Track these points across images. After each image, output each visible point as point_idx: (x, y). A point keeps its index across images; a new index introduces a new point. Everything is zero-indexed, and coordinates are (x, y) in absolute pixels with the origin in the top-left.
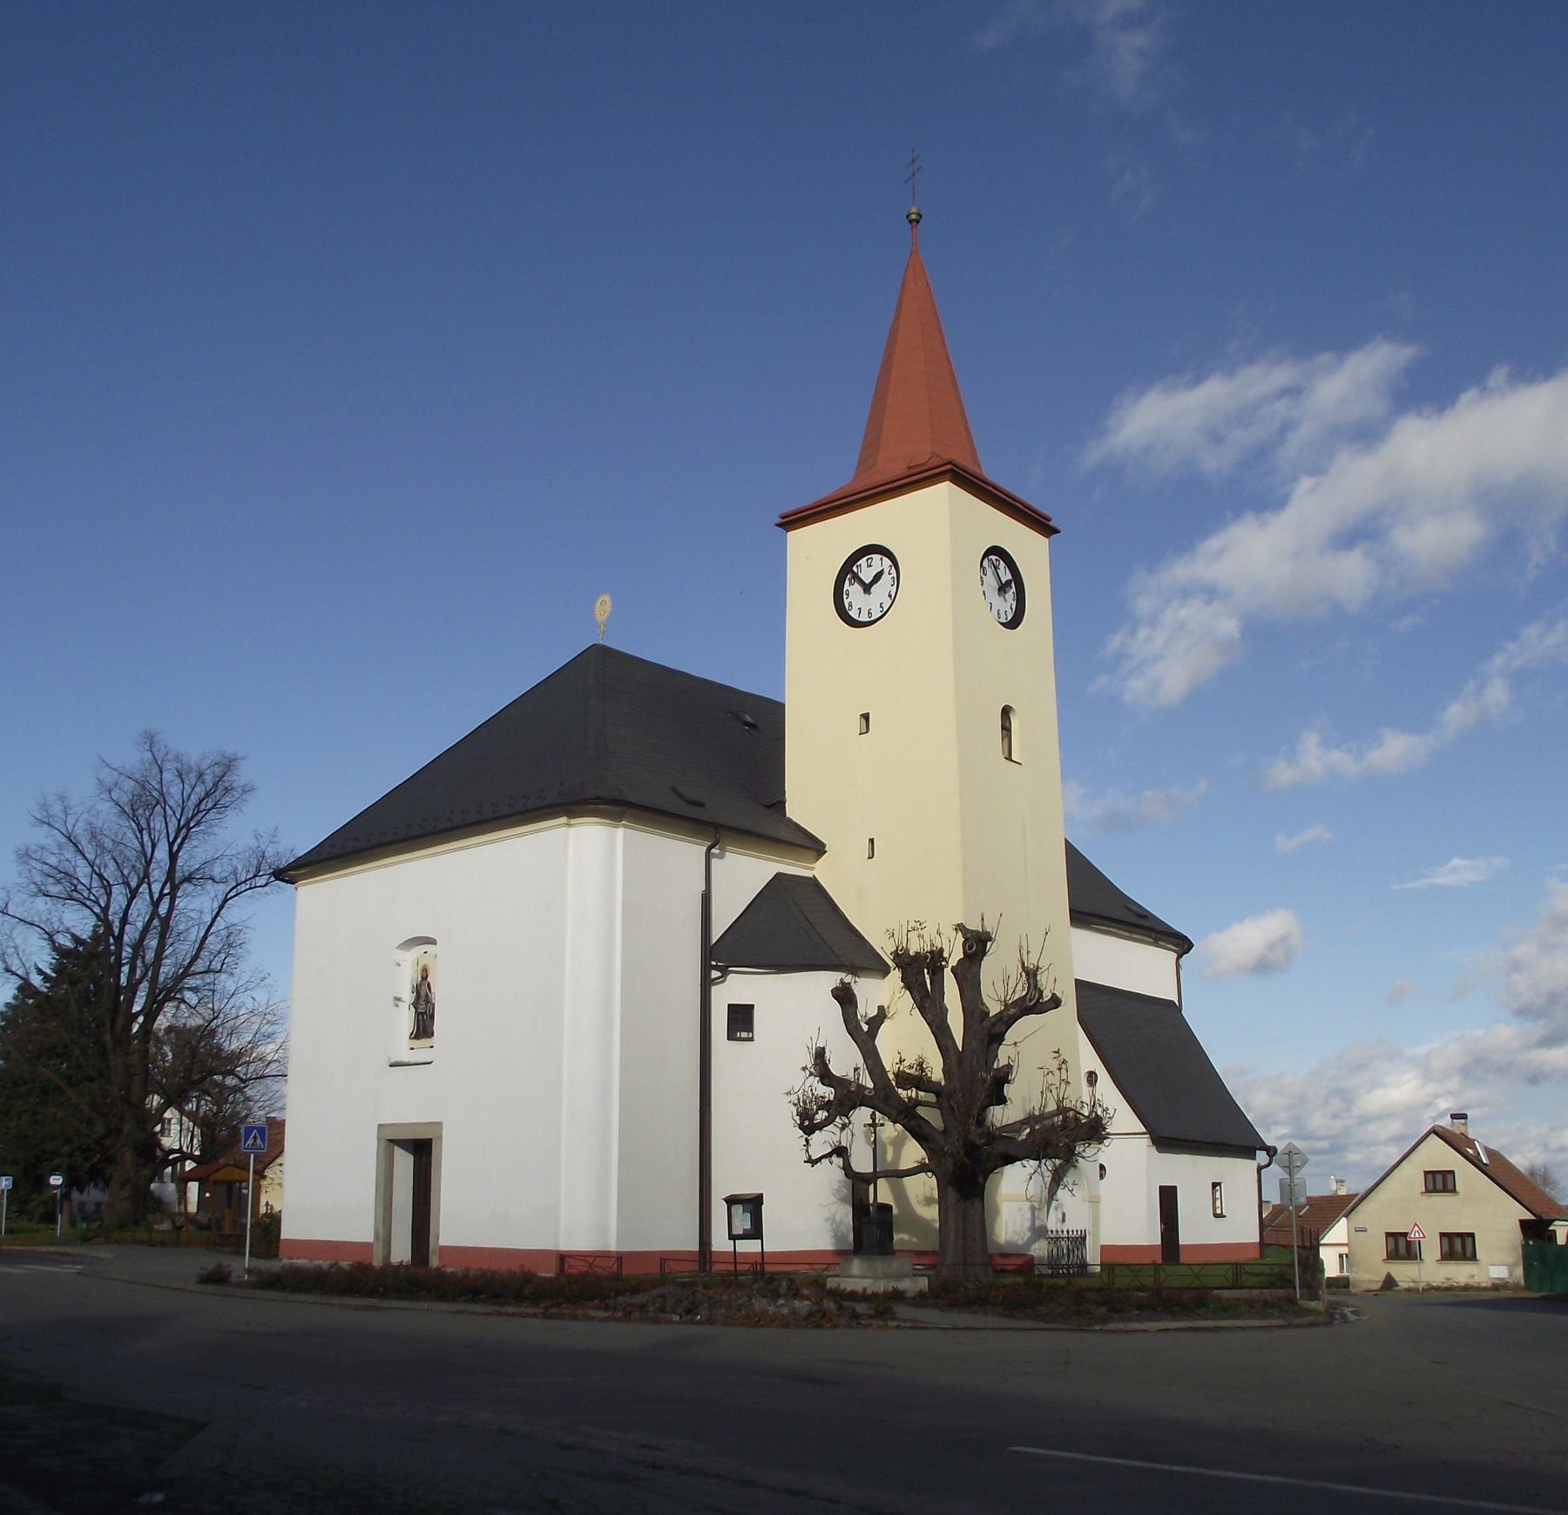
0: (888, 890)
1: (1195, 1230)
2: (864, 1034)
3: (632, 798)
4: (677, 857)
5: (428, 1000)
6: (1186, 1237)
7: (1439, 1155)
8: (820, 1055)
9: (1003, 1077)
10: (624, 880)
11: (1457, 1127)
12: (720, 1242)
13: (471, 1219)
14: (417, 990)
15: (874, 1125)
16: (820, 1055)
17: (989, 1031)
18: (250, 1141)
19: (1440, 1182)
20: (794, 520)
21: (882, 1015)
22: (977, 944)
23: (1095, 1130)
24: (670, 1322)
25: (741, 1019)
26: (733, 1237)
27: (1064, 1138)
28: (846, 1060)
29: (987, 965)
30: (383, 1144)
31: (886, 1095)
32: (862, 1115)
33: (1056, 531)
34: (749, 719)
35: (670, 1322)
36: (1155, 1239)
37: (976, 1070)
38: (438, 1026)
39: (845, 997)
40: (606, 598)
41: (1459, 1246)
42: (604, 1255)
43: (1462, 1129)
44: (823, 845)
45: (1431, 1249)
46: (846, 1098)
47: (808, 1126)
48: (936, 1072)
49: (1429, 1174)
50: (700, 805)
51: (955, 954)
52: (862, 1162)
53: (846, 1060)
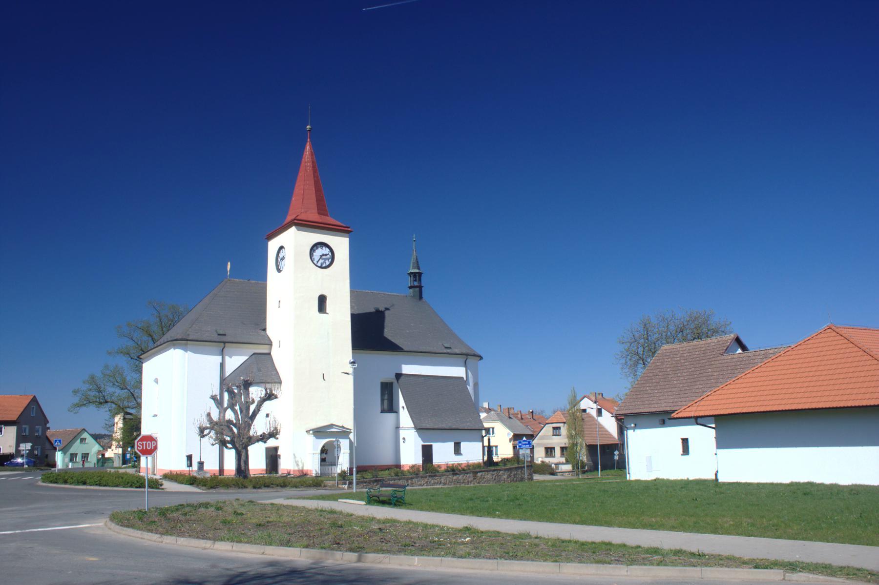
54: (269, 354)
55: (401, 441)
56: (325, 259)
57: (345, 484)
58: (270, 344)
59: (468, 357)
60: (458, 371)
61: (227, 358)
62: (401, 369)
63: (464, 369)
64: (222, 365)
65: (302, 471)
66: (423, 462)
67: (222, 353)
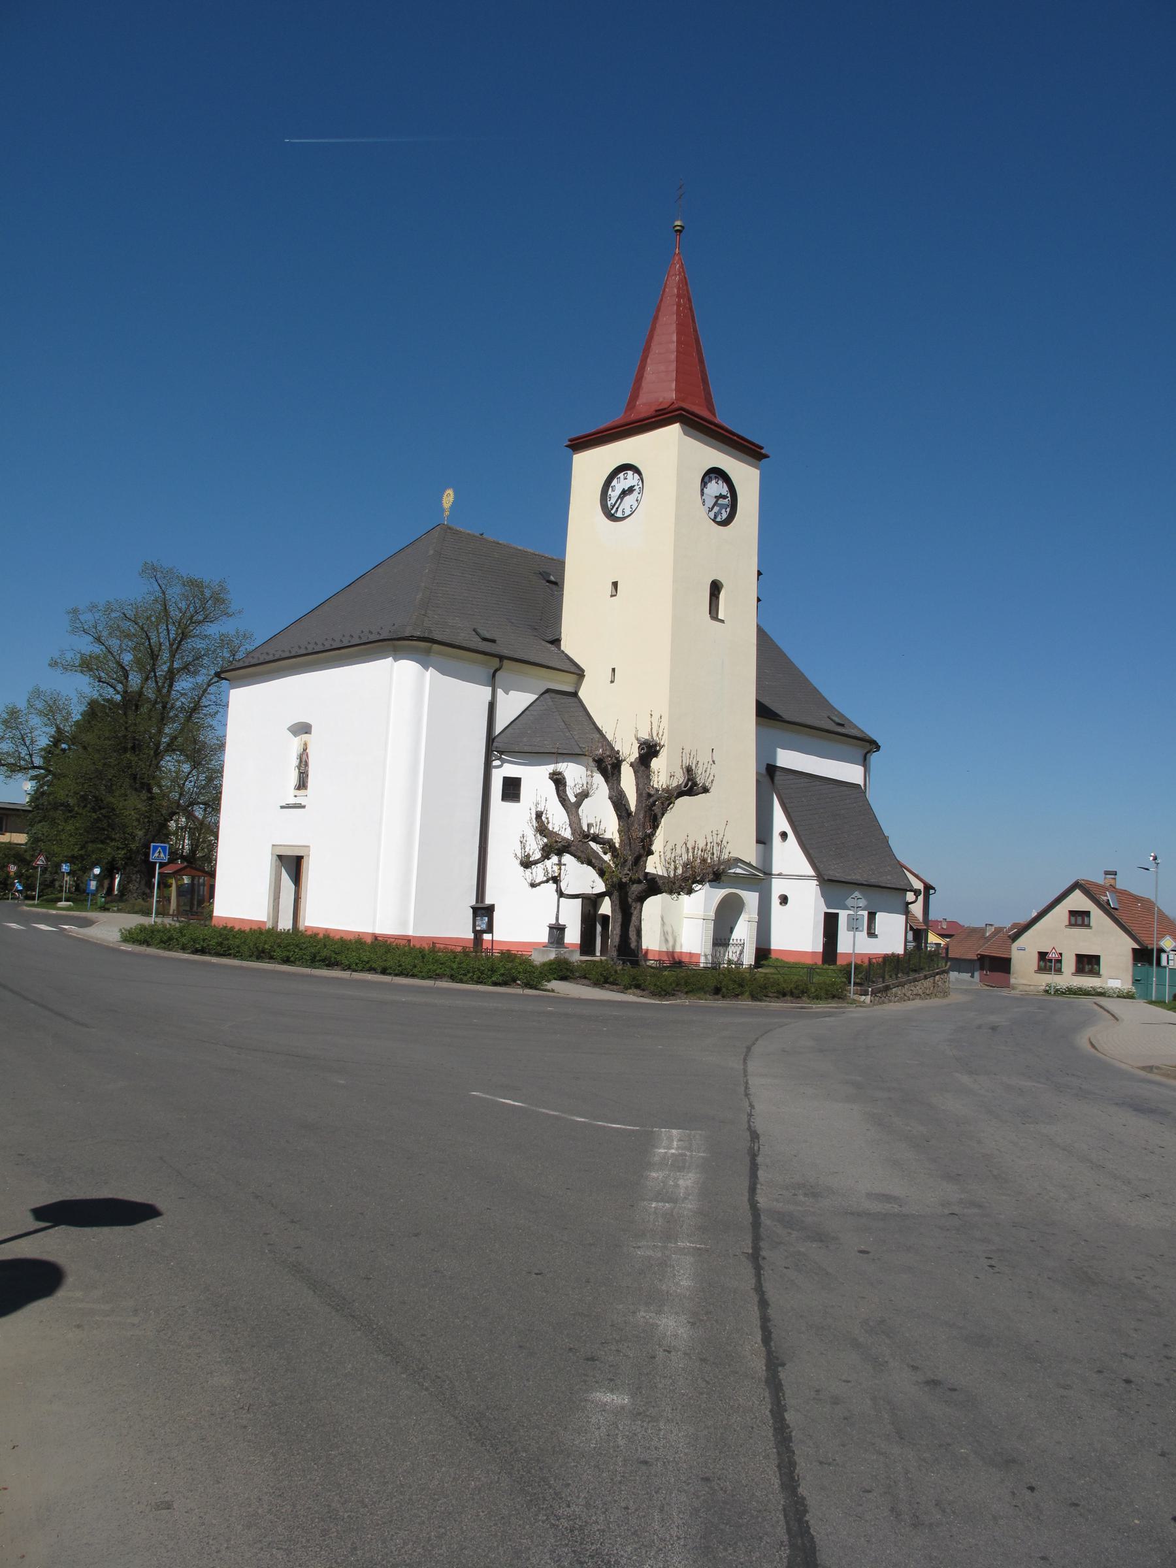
0: (619, 710)
1: (851, 943)
5: (306, 764)
7: (1078, 901)
13: (330, 909)
14: (300, 758)
16: (539, 815)
19: (1079, 918)
20: (581, 444)
21: (583, 795)
24: (862, 1005)
25: (512, 789)
29: (655, 763)
30: (275, 858)
31: (580, 845)
33: (766, 456)
34: (552, 578)
35: (862, 1005)
39: (559, 781)
41: (1088, 963)
42: (408, 939)
43: (1112, 882)
44: (583, 671)
45: (1069, 965)
46: (555, 847)
47: (527, 864)
50: (493, 641)
54: (575, 694)
55: (775, 901)
56: (722, 506)
57: (866, 994)
58: (580, 674)
59: (864, 747)
60: (851, 773)
61: (500, 692)
62: (774, 756)
63: (860, 769)
64: (492, 706)
65: (672, 954)
66: (824, 945)
67: (492, 682)
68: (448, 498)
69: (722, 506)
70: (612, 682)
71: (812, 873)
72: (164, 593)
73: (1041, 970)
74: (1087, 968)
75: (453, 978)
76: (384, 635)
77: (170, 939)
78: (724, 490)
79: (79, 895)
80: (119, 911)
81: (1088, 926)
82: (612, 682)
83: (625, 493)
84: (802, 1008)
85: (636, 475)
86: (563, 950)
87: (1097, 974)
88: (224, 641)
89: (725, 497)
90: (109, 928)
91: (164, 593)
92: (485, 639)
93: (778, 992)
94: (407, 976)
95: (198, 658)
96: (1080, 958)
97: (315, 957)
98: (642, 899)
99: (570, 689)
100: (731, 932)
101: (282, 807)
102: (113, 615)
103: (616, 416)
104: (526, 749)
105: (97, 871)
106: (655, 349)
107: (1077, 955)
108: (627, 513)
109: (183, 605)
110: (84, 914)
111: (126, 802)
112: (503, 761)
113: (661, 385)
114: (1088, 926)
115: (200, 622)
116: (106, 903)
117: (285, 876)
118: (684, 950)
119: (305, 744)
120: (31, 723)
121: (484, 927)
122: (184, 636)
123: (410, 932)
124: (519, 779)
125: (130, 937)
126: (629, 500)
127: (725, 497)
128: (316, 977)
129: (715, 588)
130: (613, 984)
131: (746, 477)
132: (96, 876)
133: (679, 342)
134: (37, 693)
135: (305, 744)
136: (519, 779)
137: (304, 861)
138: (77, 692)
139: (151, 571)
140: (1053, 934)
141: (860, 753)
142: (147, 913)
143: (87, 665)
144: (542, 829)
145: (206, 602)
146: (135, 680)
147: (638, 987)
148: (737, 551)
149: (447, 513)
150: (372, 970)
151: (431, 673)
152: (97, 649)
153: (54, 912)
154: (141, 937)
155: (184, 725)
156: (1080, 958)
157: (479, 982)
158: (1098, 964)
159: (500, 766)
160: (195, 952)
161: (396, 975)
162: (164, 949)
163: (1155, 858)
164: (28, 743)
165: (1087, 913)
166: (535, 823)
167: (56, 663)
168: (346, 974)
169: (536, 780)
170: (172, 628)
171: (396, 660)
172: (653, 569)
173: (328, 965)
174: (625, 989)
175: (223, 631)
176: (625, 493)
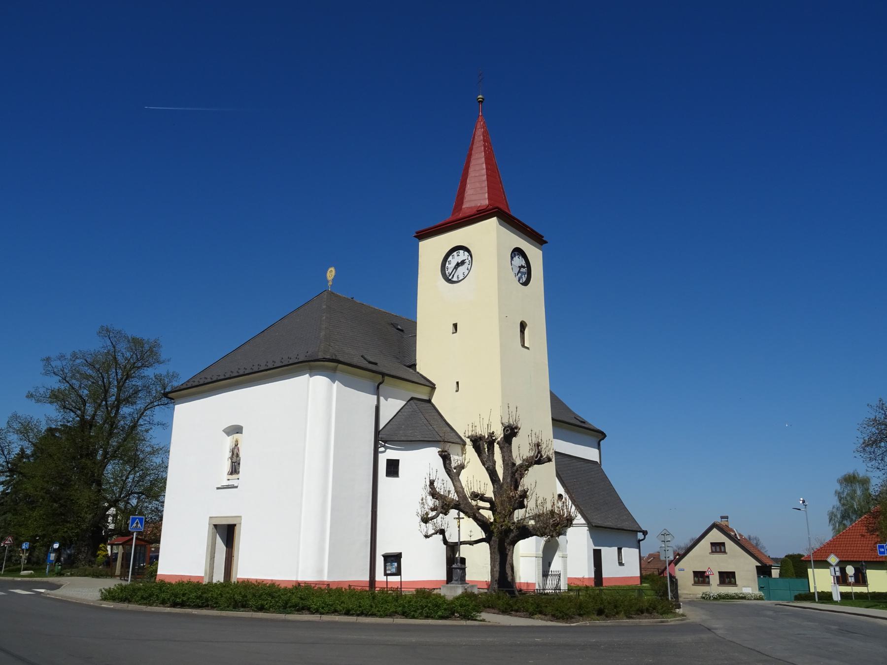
0: (468, 408)
1: (611, 570)
2: (453, 472)
3: (341, 359)
4: (363, 402)
5: (238, 455)
6: (605, 574)
7: (716, 536)
8: (432, 483)
9: (524, 495)
10: (336, 413)
11: (723, 522)
12: (380, 577)
13: (251, 566)
15: (459, 518)
16: (432, 483)
17: (516, 472)
18: (135, 525)
21: (462, 467)
22: (511, 432)
23: (569, 521)
25: (393, 468)
26: (386, 575)
27: (552, 527)
28: (445, 485)
32: (453, 513)
33: (546, 242)
36: (367, 578)
37: (510, 489)
38: (242, 468)
39: (445, 458)
40: (332, 269)
41: (727, 578)
42: (322, 583)
45: (715, 579)
46: (445, 506)
47: (425, 520)
48: (490, 494)
49: (713, 544)
50: (376, 364)
51: (499, 434)
52: (452, 538)
53: (445, 485)
56: (523, 273)
58: (433, 387)
59: (597, 437)
60: (590, 453)
61: (382, 398)
63: (597, 451)
67: (377, 392)
68: (331, 273)
69: (523, 273)
70: (457, 391)
71: (584, 522)
72: (114, 347)
73: (696, 583)
74: (727, 580)
75: (405, 614)
76: (302, 358)
77: (151, 595)
78: (523, 263)
79: (36, 564)
80: (72, 575)
81: (725, 552)
82: (457, 391)
83: (458, 265)
84: (662, 622)
85: (466, 253)
86: (466, 586)
87: (735, 584)
88: (159, 378)
89: (524, 267)
90: (84, 589)
91: (114, 347)
92: (370, 362)
93: (638, 610)
94: (366, 615)
95: (136, 392)
96: (721, 574)
97: (287, 603)
98: (514, 543)
99: (426, 397)
100: (550, 566)
101: (218, 488)
102: (78, 361)
103: (448, 217)
104: (403, 438)
105: (56, 546)
106: (472, 173)
107: (694, 572)
108: (461, 277)
109: (128, 355)
110: (45, 579)
111: (85, 492)
112: (386, 448)
113: (477, 194)
114: (725, 552)
115: (139, 368)
116: (61, 569)
117: (219, 541)
118: (522, 581)
119: (237, 441)
120: (9, 439)
121: (394, 570)
122: (128, 377)
123: (325, 578)
124: (398, 461)
125: (109, 596)
126: (462, 270)
127: (524, 267)
128: (289, 621)
129: (523, 326)
130: (517, 611)
131: (535, 254)
132: (55, 550)
133: (487, 169)
134: (15, 417)
135: (237, 441)
136: (398, 461)
137: (237, 528)
138: (47, 416)
139: (106, 332)
140: (699, 558)
141: (596, 440)
142: (112, 575)
143: (55, 397)
144: (434, 494)
145: (144, 353)
146: (90, 409)
147: (541, 613)
148: (533, 301)
149: (330, 283)
150: (335, 612)
151: (336, 385)
152: (64, 386)
153: (19, 579)
154: (124, 595)
155: (125, 440)
156: (721, 574)
157: (427, 617)
158: (734, 577)
159: (384, 452)
160: (175, 605)
161: (358, 615)
162: (145, 604)
163: (804, 502)
164: (6, 453)
165: (723, 544)
166: (429, 489)
167: (32, 396)
168: (315, 618)
169: (407, 458)
170: (120, 372)
171: (311, 376)
172: (478, 315)
173: (298, 610)
174: (531, 615)
175: (157, 372)
176: (458, 265)
